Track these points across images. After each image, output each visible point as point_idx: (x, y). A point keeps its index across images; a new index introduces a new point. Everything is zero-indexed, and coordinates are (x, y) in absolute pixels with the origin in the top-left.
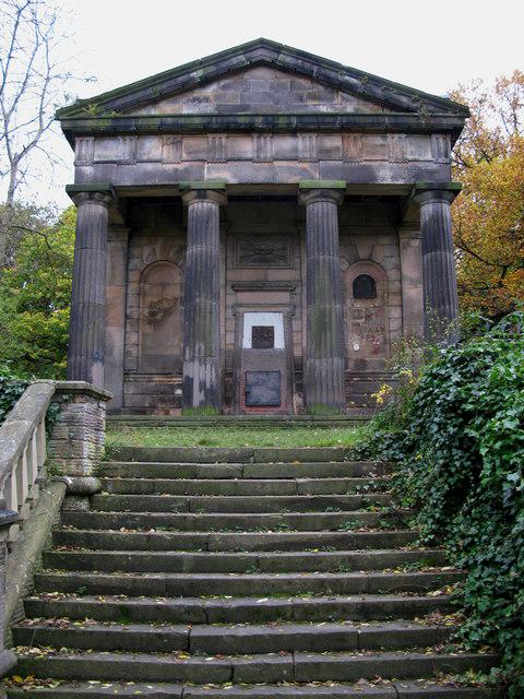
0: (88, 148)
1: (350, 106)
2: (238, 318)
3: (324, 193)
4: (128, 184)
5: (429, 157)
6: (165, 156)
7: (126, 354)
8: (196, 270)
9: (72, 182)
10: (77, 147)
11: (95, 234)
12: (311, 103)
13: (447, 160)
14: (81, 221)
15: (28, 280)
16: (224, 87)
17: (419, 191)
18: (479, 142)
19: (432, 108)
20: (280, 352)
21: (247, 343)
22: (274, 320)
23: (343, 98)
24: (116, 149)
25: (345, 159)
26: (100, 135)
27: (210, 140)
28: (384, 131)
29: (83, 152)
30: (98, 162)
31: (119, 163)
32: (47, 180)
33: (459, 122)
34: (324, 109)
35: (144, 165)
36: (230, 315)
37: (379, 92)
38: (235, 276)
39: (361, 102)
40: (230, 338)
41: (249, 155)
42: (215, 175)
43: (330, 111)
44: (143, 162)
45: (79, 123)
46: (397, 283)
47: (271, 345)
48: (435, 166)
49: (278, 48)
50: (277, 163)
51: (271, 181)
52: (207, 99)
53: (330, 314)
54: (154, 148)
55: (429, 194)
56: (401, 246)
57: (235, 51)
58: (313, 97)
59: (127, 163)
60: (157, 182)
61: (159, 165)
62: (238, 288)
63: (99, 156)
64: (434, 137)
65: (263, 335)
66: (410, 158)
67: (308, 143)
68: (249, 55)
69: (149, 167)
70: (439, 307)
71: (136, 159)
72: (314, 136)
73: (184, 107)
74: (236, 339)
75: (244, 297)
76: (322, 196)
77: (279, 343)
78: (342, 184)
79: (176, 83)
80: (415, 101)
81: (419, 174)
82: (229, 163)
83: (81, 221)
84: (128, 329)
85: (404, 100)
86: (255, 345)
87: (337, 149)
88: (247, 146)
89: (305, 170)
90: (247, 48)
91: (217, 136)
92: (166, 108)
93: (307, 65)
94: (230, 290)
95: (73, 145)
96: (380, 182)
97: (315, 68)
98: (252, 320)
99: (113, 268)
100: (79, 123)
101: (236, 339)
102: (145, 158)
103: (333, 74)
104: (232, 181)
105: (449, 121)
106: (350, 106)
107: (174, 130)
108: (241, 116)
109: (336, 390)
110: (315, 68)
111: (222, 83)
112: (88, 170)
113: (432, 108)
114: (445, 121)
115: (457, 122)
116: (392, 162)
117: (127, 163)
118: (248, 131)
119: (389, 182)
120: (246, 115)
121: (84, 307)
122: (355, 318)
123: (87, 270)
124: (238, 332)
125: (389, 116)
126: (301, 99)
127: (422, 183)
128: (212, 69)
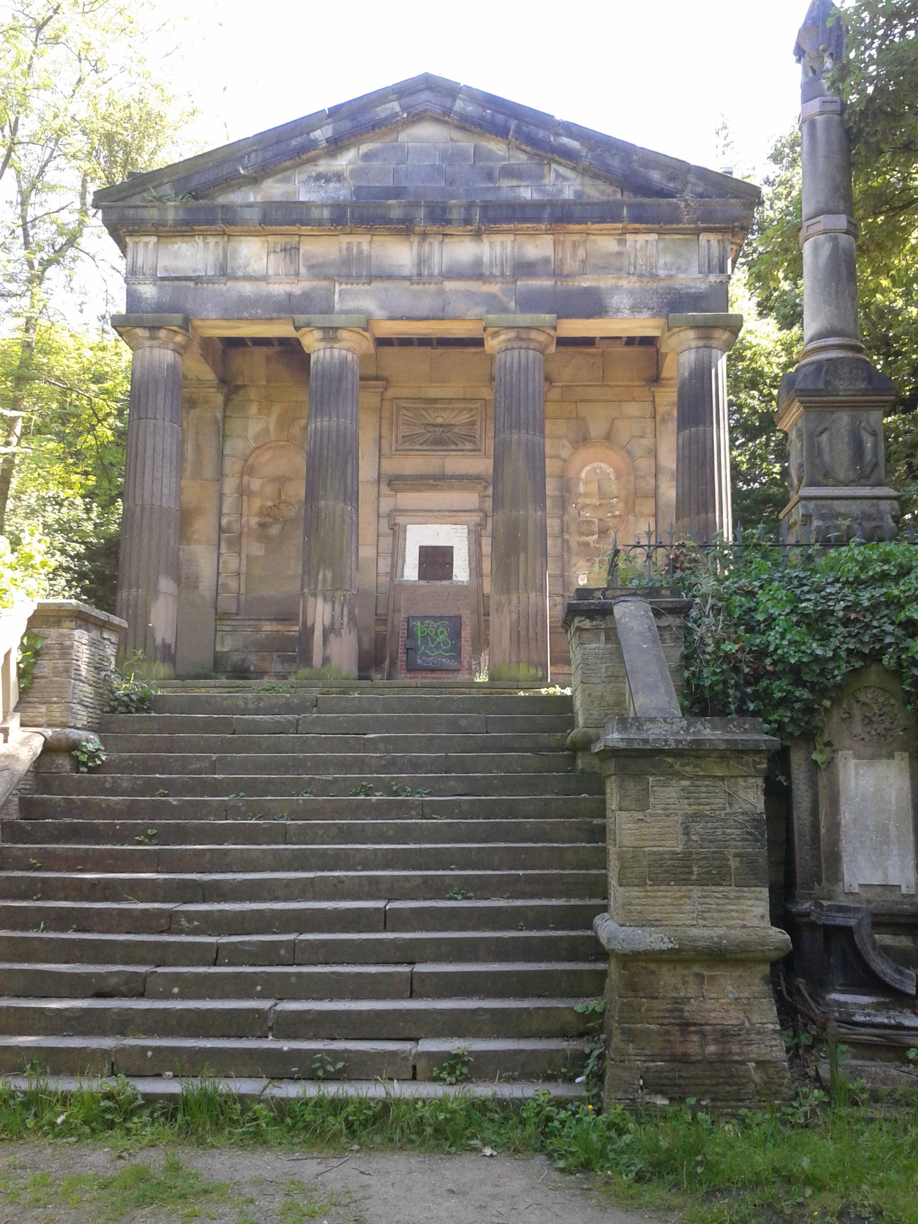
0: (146, 249)
2: (397, 533)
7: (218, 588)
8: (321, 455)
9: (121, 308)
10: (129, 254)
11: (160, 396)
12: (505, 183)
14: (138, 374)
15: (53, 1124)
16: (367, 157)
20: (461, 587)
21: (411, 571)
22: (453, 536)
24: (192, 256)
26: (164, 232)
29: (140, 262)
30: (163, 279)
31: (197, 280)
32: (84, 306)
36: (384, 525)
38: (391, 466)
39: (588, 181)
40: (384, 565)
42: (351, 304)
44: (237, 279)
45: (132, 206)
46: (652, 481)
47: (449, 575)
49: (450, 90)
50: (449, 285)
52: (339, 177)
53: (526, 523)
56: (658, 418)
57: (381, 97)
59: (210, 280)
62: (397, 482)
63: (166, 270)
65: (436, 561)
68: (408, 100)
71: (224, 272)
73: (299, 188)
74: (394, 565)
75: (410, 499)
77: (461, 571)
79: (284, 148)
80: (671, 178)
83: (138, 374)
84: (223, 550)
86: (422, 576)
89: (493, 296)
90: (402, 91)
92: (273, 189)
94: (385, 489)
95: (123, 248)
98: (420, 536)
99: (198, 450)
100: (132, 206)
101: (394, 565)
102: (240, 273)
107: (284, 219)
109: (533, 643)
112: (148, 291)
117: (210, 280)
121: (142, 512)
122: (581, 534)
123: (149, 453)
124: (397, 555)
126: (490, 177)
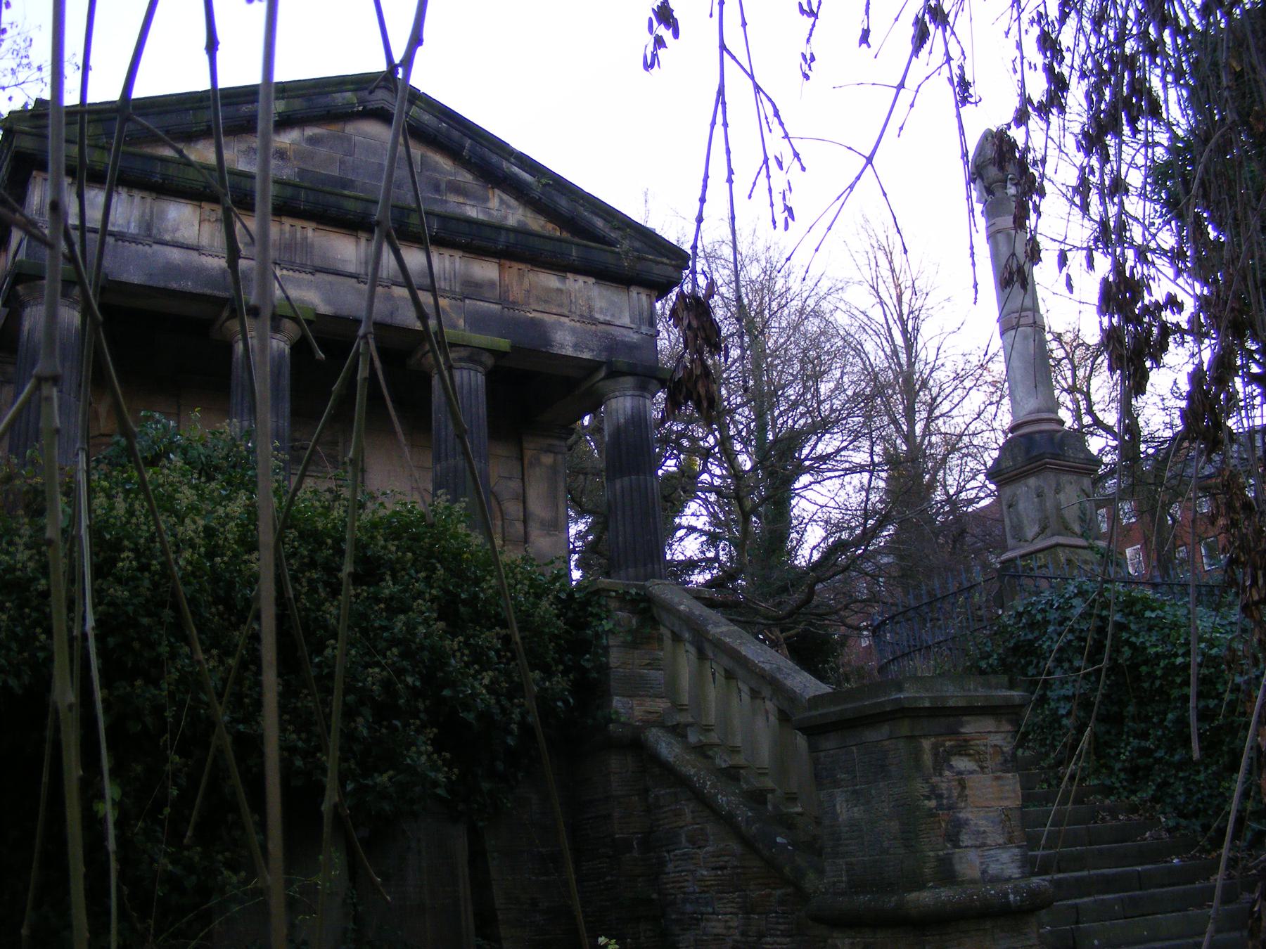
1: (515, 215)
3: (474, 355)
4: (136, 280)
5: (626, 320)
6: (205, 241)
12: (453, 198)
13: (652, 332)
16: (312, 140)
17: (614, 374)
18: (480, 363)
19: (637, 244)
23: (502, 201)
25: (503, 300)
27: (287, 227)
28: (562, 267)
33: (675, 274)
34: (472, 212)
35: (167, 249)
37: (563, 203)
41: (351, 268)
43: (481, 217)
48: (635, 337)
51: (388, 321)
54: (183, 220)
55: (628, 381)
58: (456, 189)
59: (134, 240)
60: (189, 286)
61: (194, 254)
64: (634, 291)
66: (601, 317)
67: (447, 264)
69: (176, 255)
70: (645, 565)
72: (457, 255)
76: (470, 359)
78: (504, 344)
81: (614, 346)
82: (318, 275)
85: (599, 223)
87: (492, 284)
88: (347, 250)
91: (299, 224)
93: (456, 134)
96: (556, 350)
97: (468, 143)
103: (495, 159)
104: (324, 309)
105: (662, 270)
106: (515, 215)
107: (225, 195)
108: (349, 197)
110: (468, 143)
111: (310, 131)
113: (637, 244)
114: (657, 270)
115: (670, 271)
116: (576, 313)
117: (134, 240)
118: (354, 224)
119: (569, 352)
120: (357, 198)
125: (578, 245)
127: (621, 360)
128: (298, 104)
